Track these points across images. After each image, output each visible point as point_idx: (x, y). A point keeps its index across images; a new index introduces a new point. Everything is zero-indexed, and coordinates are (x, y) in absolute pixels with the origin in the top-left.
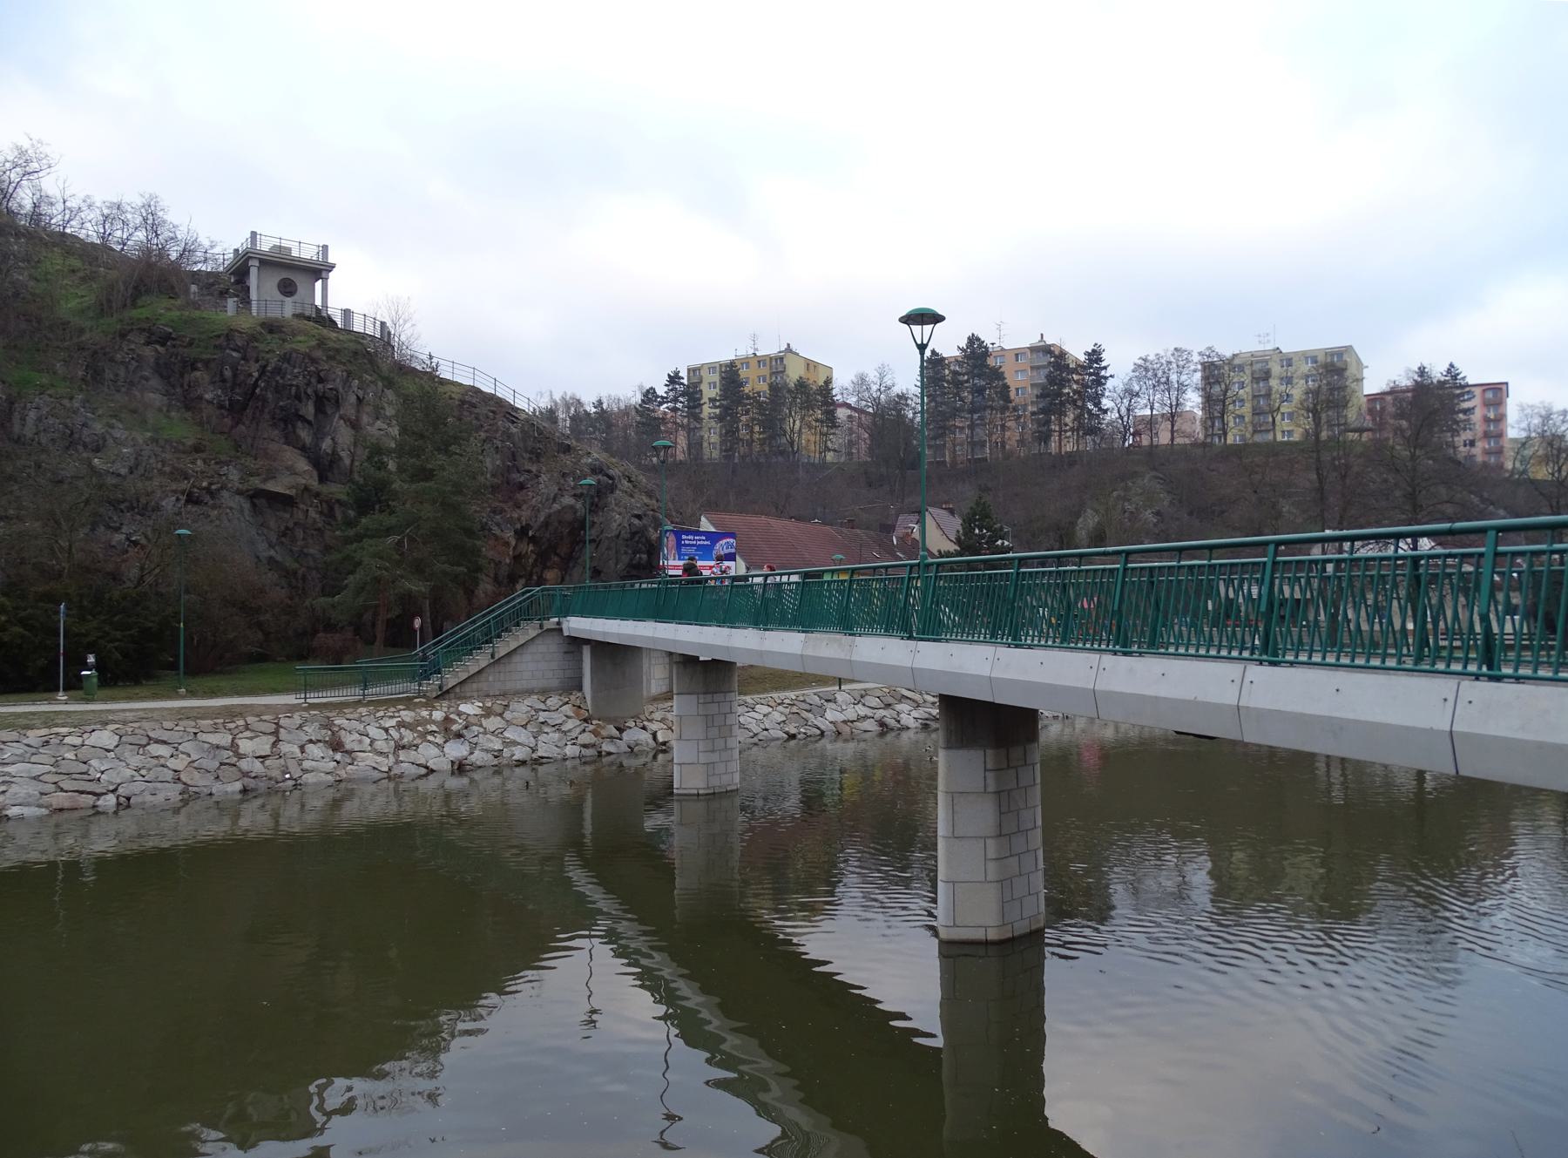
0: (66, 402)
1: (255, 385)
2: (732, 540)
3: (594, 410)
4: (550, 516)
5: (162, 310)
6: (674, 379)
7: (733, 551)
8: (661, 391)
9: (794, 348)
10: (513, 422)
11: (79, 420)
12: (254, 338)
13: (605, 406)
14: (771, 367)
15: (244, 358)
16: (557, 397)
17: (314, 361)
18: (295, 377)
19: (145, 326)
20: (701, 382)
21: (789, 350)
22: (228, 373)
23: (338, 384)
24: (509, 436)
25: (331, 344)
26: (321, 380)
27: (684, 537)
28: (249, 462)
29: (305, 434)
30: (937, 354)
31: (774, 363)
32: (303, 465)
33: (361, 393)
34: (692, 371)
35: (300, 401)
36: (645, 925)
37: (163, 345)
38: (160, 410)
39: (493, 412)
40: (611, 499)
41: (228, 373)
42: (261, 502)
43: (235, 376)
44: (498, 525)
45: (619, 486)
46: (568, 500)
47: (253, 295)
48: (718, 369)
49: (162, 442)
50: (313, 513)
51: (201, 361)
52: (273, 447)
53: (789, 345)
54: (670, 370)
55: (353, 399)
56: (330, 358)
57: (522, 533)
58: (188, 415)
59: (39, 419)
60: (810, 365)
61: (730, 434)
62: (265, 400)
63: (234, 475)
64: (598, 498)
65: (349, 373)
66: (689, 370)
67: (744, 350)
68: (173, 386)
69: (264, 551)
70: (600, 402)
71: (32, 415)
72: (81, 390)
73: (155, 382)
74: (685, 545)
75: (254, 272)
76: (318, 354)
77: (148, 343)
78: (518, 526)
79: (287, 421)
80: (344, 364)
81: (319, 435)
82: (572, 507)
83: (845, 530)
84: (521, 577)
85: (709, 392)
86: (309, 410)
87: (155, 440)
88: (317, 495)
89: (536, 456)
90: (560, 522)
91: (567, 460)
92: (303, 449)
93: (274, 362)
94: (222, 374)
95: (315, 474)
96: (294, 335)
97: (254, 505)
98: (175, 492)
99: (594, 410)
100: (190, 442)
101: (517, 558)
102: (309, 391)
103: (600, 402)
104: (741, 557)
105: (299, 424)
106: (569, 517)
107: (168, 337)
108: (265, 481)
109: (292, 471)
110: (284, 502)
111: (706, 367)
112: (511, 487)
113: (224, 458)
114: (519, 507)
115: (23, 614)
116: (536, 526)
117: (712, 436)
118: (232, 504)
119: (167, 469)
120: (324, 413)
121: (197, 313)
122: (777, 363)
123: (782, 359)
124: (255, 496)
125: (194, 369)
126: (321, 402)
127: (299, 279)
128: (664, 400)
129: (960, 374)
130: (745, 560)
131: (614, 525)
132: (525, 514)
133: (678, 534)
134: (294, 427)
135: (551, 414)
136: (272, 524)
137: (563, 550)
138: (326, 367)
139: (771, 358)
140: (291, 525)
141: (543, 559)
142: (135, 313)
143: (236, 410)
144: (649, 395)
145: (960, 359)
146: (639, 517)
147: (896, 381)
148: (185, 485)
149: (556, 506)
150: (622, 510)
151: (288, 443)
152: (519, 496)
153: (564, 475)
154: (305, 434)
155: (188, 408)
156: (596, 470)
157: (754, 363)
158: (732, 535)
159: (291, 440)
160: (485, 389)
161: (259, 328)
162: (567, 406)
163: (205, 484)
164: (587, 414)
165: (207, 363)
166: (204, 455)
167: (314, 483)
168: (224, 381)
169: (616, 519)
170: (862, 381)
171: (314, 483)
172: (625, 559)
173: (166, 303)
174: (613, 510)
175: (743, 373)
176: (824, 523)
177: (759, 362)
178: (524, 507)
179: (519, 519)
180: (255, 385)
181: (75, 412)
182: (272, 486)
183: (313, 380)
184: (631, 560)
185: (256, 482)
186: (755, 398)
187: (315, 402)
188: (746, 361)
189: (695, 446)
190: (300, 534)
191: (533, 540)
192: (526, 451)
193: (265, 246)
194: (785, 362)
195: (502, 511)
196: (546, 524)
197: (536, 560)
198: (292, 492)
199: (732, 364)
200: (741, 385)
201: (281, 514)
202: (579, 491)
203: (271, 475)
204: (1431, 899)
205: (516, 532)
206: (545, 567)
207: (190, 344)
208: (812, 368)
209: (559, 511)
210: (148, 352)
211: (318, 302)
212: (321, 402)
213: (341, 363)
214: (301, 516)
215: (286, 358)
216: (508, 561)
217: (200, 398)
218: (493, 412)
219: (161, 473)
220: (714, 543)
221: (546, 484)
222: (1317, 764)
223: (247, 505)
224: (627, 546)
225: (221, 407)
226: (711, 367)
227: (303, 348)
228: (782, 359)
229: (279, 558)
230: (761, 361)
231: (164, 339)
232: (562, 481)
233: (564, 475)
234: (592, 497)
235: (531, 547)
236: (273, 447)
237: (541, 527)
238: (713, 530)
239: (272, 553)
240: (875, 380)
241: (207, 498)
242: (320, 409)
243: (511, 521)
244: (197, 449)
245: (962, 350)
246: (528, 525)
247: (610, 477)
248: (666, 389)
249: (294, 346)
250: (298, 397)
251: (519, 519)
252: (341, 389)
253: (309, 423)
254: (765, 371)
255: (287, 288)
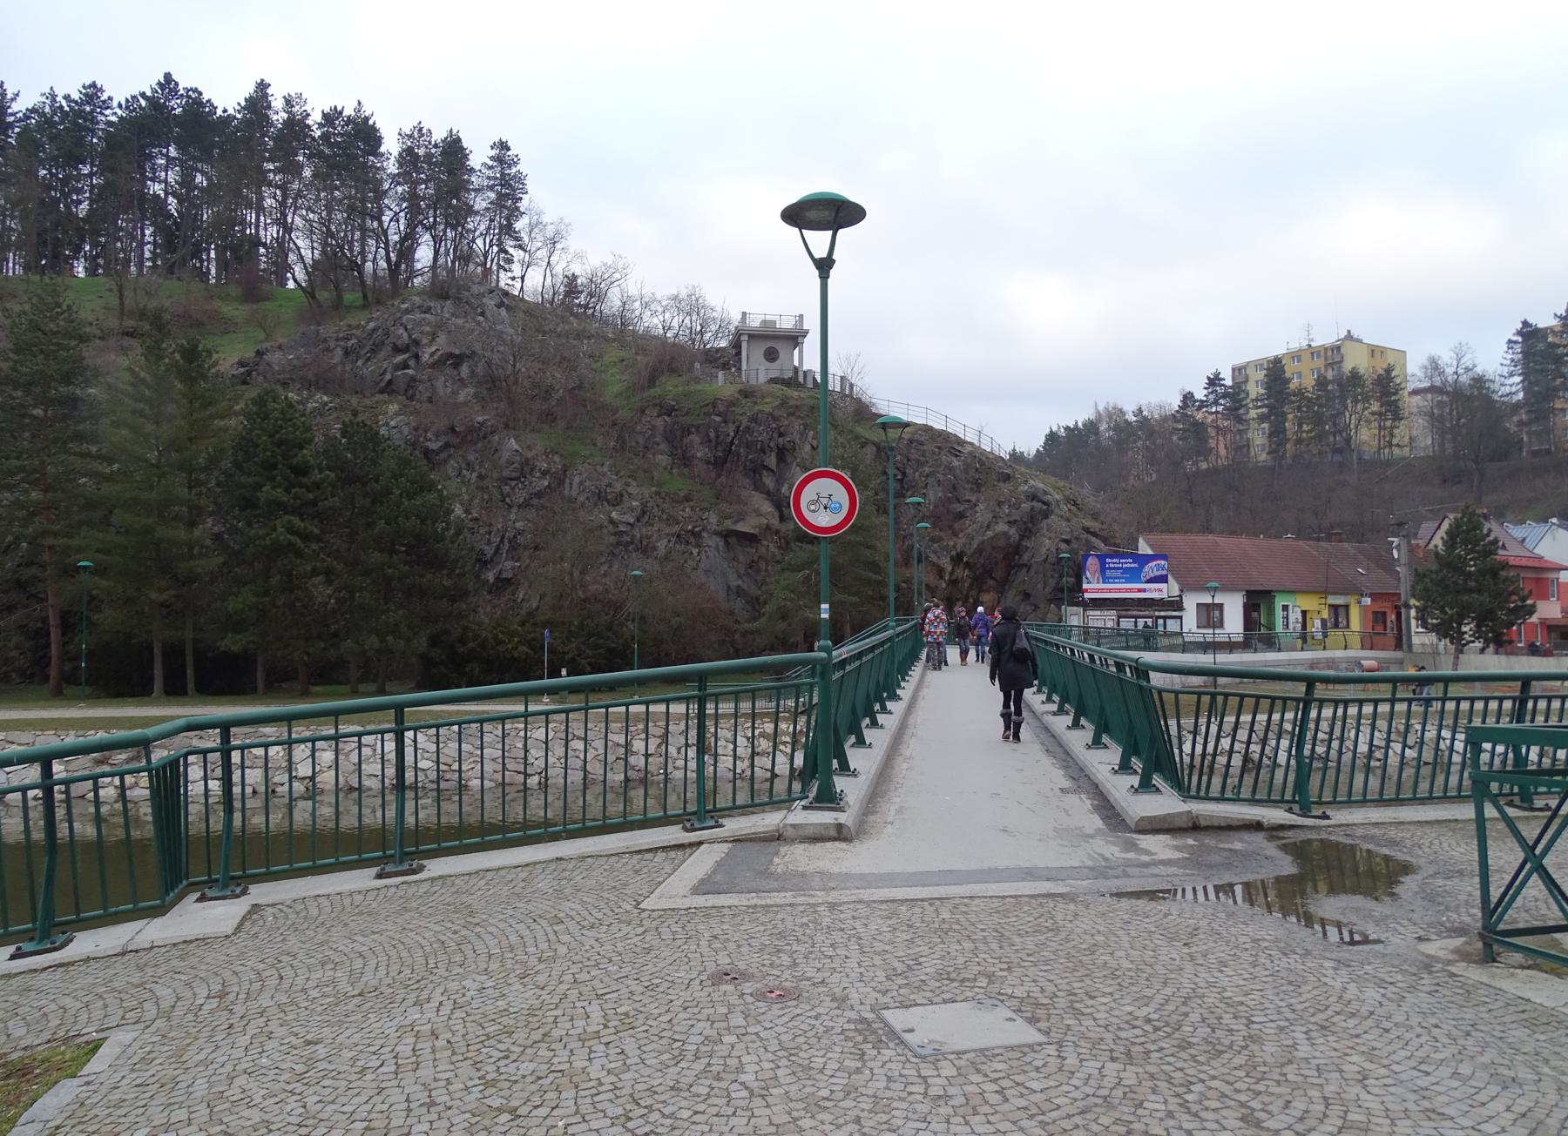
0: (598, 468)
1: (732, 443)
2: (1163, 562)
3: (1134, 419)
4: (983, 542)
5: (670, 387)
6: (1214, 381)
7: (1164, 572)
8: (1200, 394)
9: (1355, 334)
10: (956, 456)
11: (606, 481)
12: (732, 404)
13: (1145, 413)
14: (1326, 359)
15: (725, 422)
16: (1101, 408)
17: (776, 419)
18: (761, 434)
19: (658, 401)
20: (1246, 381)
21: (1349, 336)
22: (712, 435)
23: (796, 437)
24: (950, 469)
25: (792, 403)
26: (781, 435)
27: (1108, 560)
28: (724, 507)
29: (769, 481)
30: (1531, 326)
31: (1329, 353)
32: (767, 507)
33: (815, 443)
34: (1238, 370)
35: (764, 452)
36: (152, 679)
37: (669, 415)
38: (666, 468)
39: (939, 448)
40: (1044, 524)
41: (712, 435)
42: (732, 540)
43: (717, 437)
44: (935, 552)
45: (1057, 511)
46: (1002, 527)
47: (744, 367)
48: (1322, 353)
49: (663, 495)
50: (772, 548)
51: (693, 426)
52: (745, 493)
53: (1349, 332)
54: (1210, 373)
55: (808, 448)
56: (792, 414)
57: (957, 559)
58: (685, 471)
59: (581, 483)
60: (1374, 351)
61: (1277, 433)
62: (738, 455)
63: (713, 519)
64: (1029, 526)
65: (806, 426)
66: (1234, 370)
67: (1297, 342)
68: (676, 448)
69: (735, 581)
70: (1140, 410)
71: (577, 479)
72: (611, 457)
73: (663, 446)
74: (1110, 568)
75: (744, 345)
76: (782, 413)
77: (659, 416)
78: (954, 553)
79: (756, 470)
80: (802, 418)
81: (780, 481)
82: (1005, 534)
83: (1324, 544)
84: (958, 600)
85: (1254, 390)
86: (772, 461)
87: (658, 493)
88: (777, 532)
89: (977, 486)
90: (993, 548)
91: (1005, 488)
92: (768, 493)
93: (745, 422)
94: (708, 435)
95: (777, 514)
96: (763, 397)
97: (727, 543)
98: (667, 535)
99: (1134, 419)
100: (682, 494)
101: (954, 582)
102: (772, 445)
103: (1140, 410)
104: (1176, 578)
105: (765, 473)
106: (1002, 543)
107: (673, 409)
108: (736, 522)
109: (758, 514)
110: (751, 539)
111: (1252, 365)
112: (948, 517)
113: (706, 505)
114: (957, 536)
115: (529, 636)
116: (969, 553)
117: (1258, 437)
118: (711, 543)
119: (665, 516)
120: (785, 461)
121: (699, 387)
122: (1333, 353)
123: (1338, 348)
124: (727, 535)
125: (690, 433)
126: (782, 454)
127: (781, 348)
128: (1203, 404)
129: (1559, 346)
130: (1178, 581)
131: (1044, 550)
132: (960, 541)
133: (1102, 558)
134: (760, 475)
135: (1091, 426)
136: (741, 558)
137: (999, 573)
138: (786, 422)
139: (1326, 349)
140: (755, 558)
141: (979, 582)
142: (652, 392)
143: (719, 464)
144: (1188, 398)
145: (1557, 329)
146: (1067, 542)
147: (1476, 361)
148: (676, 529)
149: (990, 534)
150: (1052, 535)
151: (756, 489)
152: (956, 526)
153: (1000, 504)
154: (769, 481)
155: (686, 465)
156: (1033, 497)
157: (1306, 357)
158: (1164, 557)
159: (758, 487)
160: (937, 426)
161: (737, 395)
162: (1110, 416)
163: (690, 527)
164: (1128, 423)
165: (698, 427)
166: (692, 504)
167: (775, 522)
168: (710, 441)
169: (1045, 544)
170: (1434, 366)
171: (775, 522)
172: (1052, 583)
173: (674, 380)
174: (1044, 536)
175: (1290, 369)
176: (1299, 538)
177: (1312, 354)
178: (961, 535)
179: (954, 547)
180: (732, 443)
181: (604, 475)
182: (743, 527)
183: (775, 435)
184: (1058, 583)
185: (729, 524)
186: (1300, 392)
187: (777, 454)
188: (1296, 356)
189: (1242, 448)
190: (763, 565)
191: (967, 565)
192: (968, 482)
193: (755, 323)
194: (1342, 351)
195: (940, 539)
196: (980, 551)
197: (971, 584)
198: (756, 531)
199: (1277, 361)
200: (1288, 381)
201: (749, 549)
202: (1012, 519)
203: (741, 518)
204: (1393, 894)
205: (952, 558)
206: (980, 591)
207: (687, 414)
208: (1377, 354)
209: (992, 538)
210: (659, 422)
211: (796, 363)
212: (782, 454)
213: (799, 417)
214: (764, 550)
215: (754, 419)
216: (944, 585)
217: (694, 456)
218: (939, 448)
219: (660, 519)
220: (1142, 565)
221: (982, 513)
222: (1113, 754)
223: (721, 544)
224: (1054, 570)
225: (708, 462)
226: (1258, 365)
227: (767, 409)
228: (1338, 348)
229: (745, 587)
230: (1313, 352)
231: (670, 411)
232: (997, 509)
233: (1000, 504)
234: (1025, 523)
235: (967, 572)
236: (745, 493)
237: (974, 553)
238: (1150, 552)
239: (740, 582)
240: (1449, 362)
241: (692, 540)
242: (781, 458)
243: (947, 548)
244: (687, 499)
245: (1561, 317)
246: (962, 552)
247: (1045, 503)
248: (1205, 392)
249: (760, 408)
250: (763, 451)
251: (954, 547)
252: (798, 441)
253: (772, 471)
254: (1319, 363)
255: (771, 355)
